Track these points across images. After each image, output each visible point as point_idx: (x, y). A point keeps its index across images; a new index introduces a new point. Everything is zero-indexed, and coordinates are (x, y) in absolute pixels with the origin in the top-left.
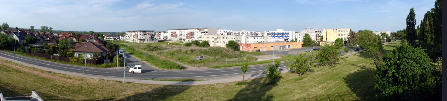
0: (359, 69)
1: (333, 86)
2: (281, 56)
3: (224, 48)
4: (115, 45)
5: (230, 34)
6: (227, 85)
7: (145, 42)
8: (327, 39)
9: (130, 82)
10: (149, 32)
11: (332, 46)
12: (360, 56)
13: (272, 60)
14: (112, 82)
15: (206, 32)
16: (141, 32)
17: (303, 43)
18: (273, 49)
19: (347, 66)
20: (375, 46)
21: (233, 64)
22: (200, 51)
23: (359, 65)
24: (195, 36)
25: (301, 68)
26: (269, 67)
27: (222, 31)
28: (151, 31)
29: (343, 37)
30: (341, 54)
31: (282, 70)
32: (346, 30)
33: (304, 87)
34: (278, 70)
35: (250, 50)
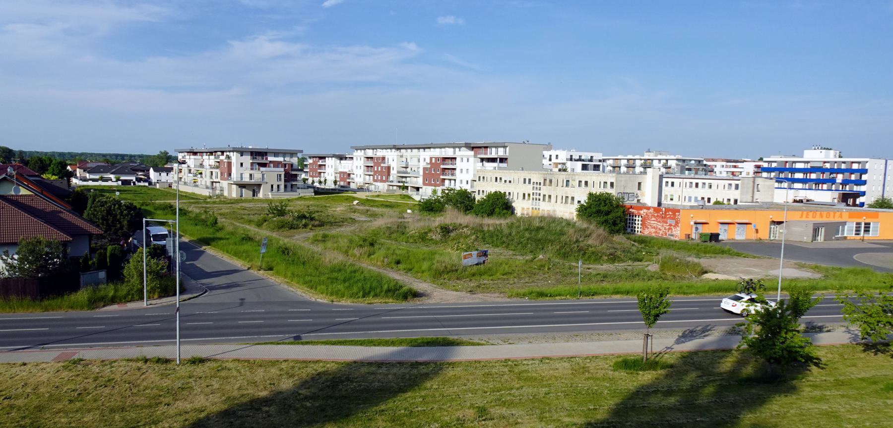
2: (816, 269)
3: (569, 223)
4: (131, 207)
5: (596, 167)
6: (580, 366)
7: (261, 195)
9: (204, 356)
10: (276, 154)
14: (121, 368)
15: (502, 160)
16: (242, 152)
18: (779, 234)
21: (605, 284)
22: (478, 230)
24: (458, 175)
27: (563, 156)
28: (284, 153)
31: (820, 329)
34: (802, 327)
35: (678, 234)
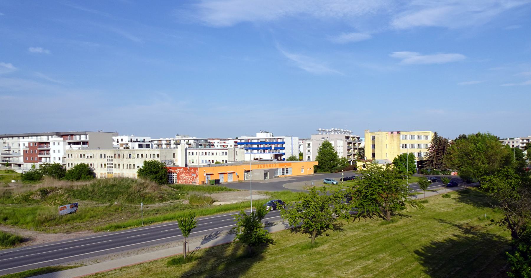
0: (458, 232)
1: (389, 268)
2: (267, 193)
3: (133, 180)
5: (148, 146)
8: (373, 155)
11: (388, 171)
12: (461, 200)
13: (248, 201)
15: (84, 143)
17: (317, 163)
18: (249, 177)
19: (425, 223)
20: (508, 177)
21: (158, 216)
22: (70, 190)
23: (458, 222)
25: (314, 221)
26: (242, 218)
29: (415, 151)
30: (412, 192)
31: (271, 224)
32: (423, 134)
33: (320, 265)
34: (263, 225)
35: (198, 182)
